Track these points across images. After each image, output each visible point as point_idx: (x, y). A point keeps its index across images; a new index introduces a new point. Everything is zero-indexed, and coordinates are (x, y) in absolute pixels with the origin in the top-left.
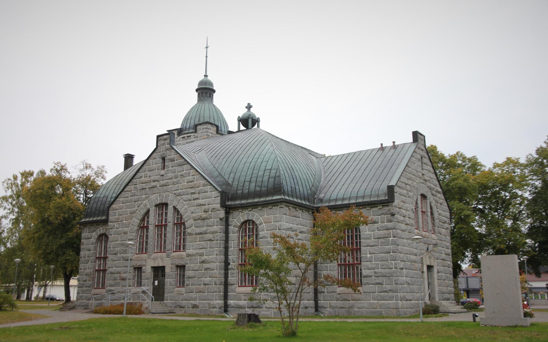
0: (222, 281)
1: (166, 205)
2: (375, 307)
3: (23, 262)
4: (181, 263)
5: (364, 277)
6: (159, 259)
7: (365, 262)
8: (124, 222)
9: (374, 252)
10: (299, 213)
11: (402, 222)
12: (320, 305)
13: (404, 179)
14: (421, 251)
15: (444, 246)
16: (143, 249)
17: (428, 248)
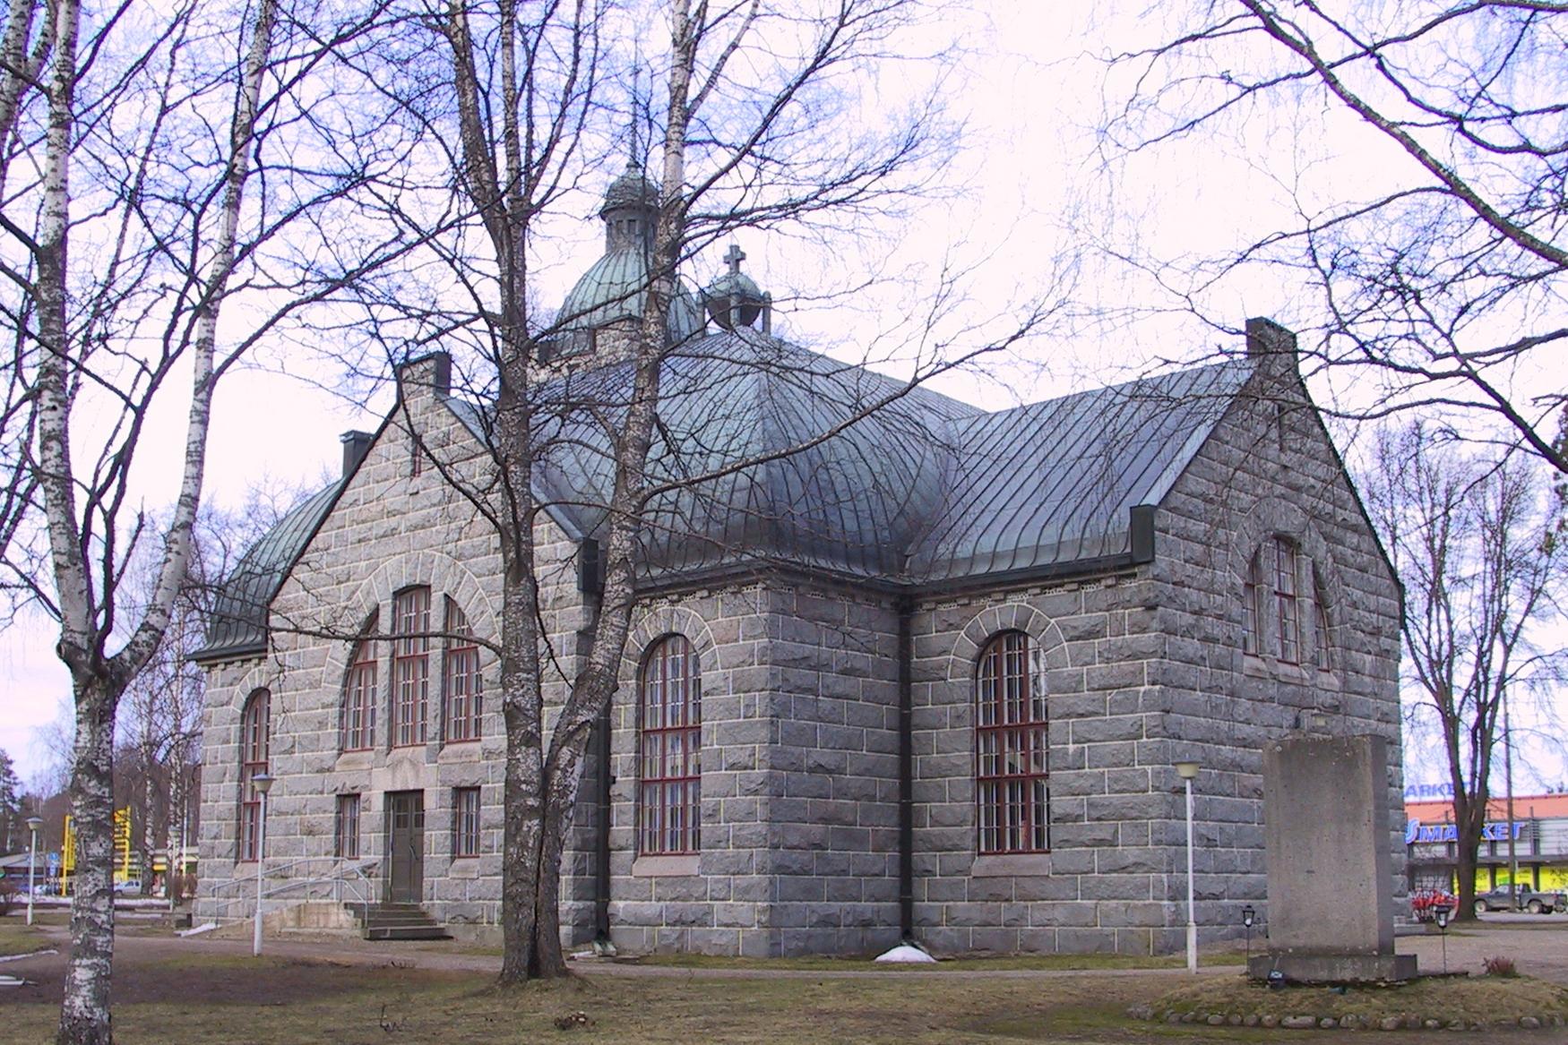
0: (587, 836)
1: (426, 588)
2: (1089, 920)
4: (468, 779)
5: (1056, 820)
6: (406, 765)
7: (1059, 769)
8: (311, 648)
9: (1092, 737)
10: (841, 608)
11: (1188, 632)
12: (916, 916)
13: (1198, 483)
14: (1269, 732)
15: (1371, 712)
16: (353, 738)
17: (1297, 719)
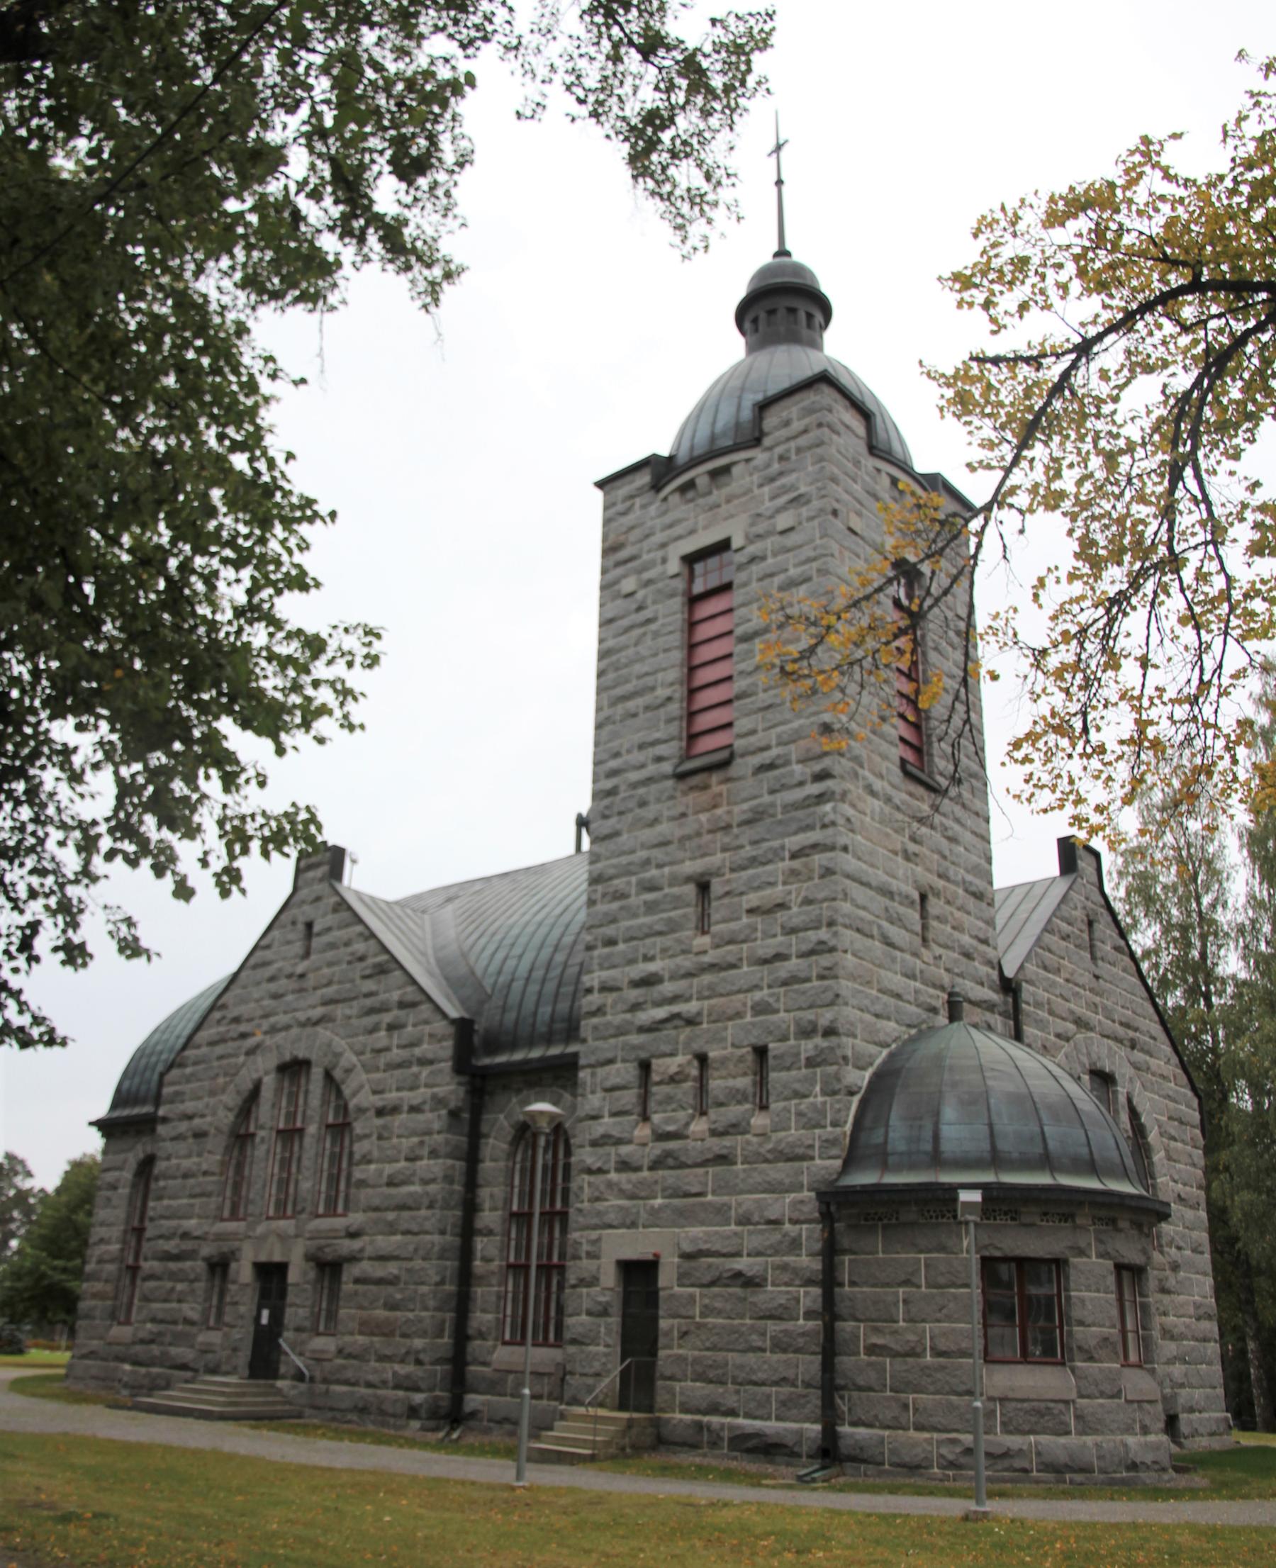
3: (50, 417)
